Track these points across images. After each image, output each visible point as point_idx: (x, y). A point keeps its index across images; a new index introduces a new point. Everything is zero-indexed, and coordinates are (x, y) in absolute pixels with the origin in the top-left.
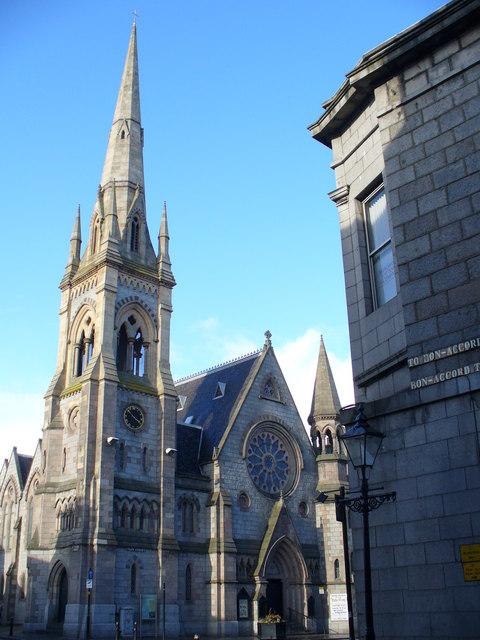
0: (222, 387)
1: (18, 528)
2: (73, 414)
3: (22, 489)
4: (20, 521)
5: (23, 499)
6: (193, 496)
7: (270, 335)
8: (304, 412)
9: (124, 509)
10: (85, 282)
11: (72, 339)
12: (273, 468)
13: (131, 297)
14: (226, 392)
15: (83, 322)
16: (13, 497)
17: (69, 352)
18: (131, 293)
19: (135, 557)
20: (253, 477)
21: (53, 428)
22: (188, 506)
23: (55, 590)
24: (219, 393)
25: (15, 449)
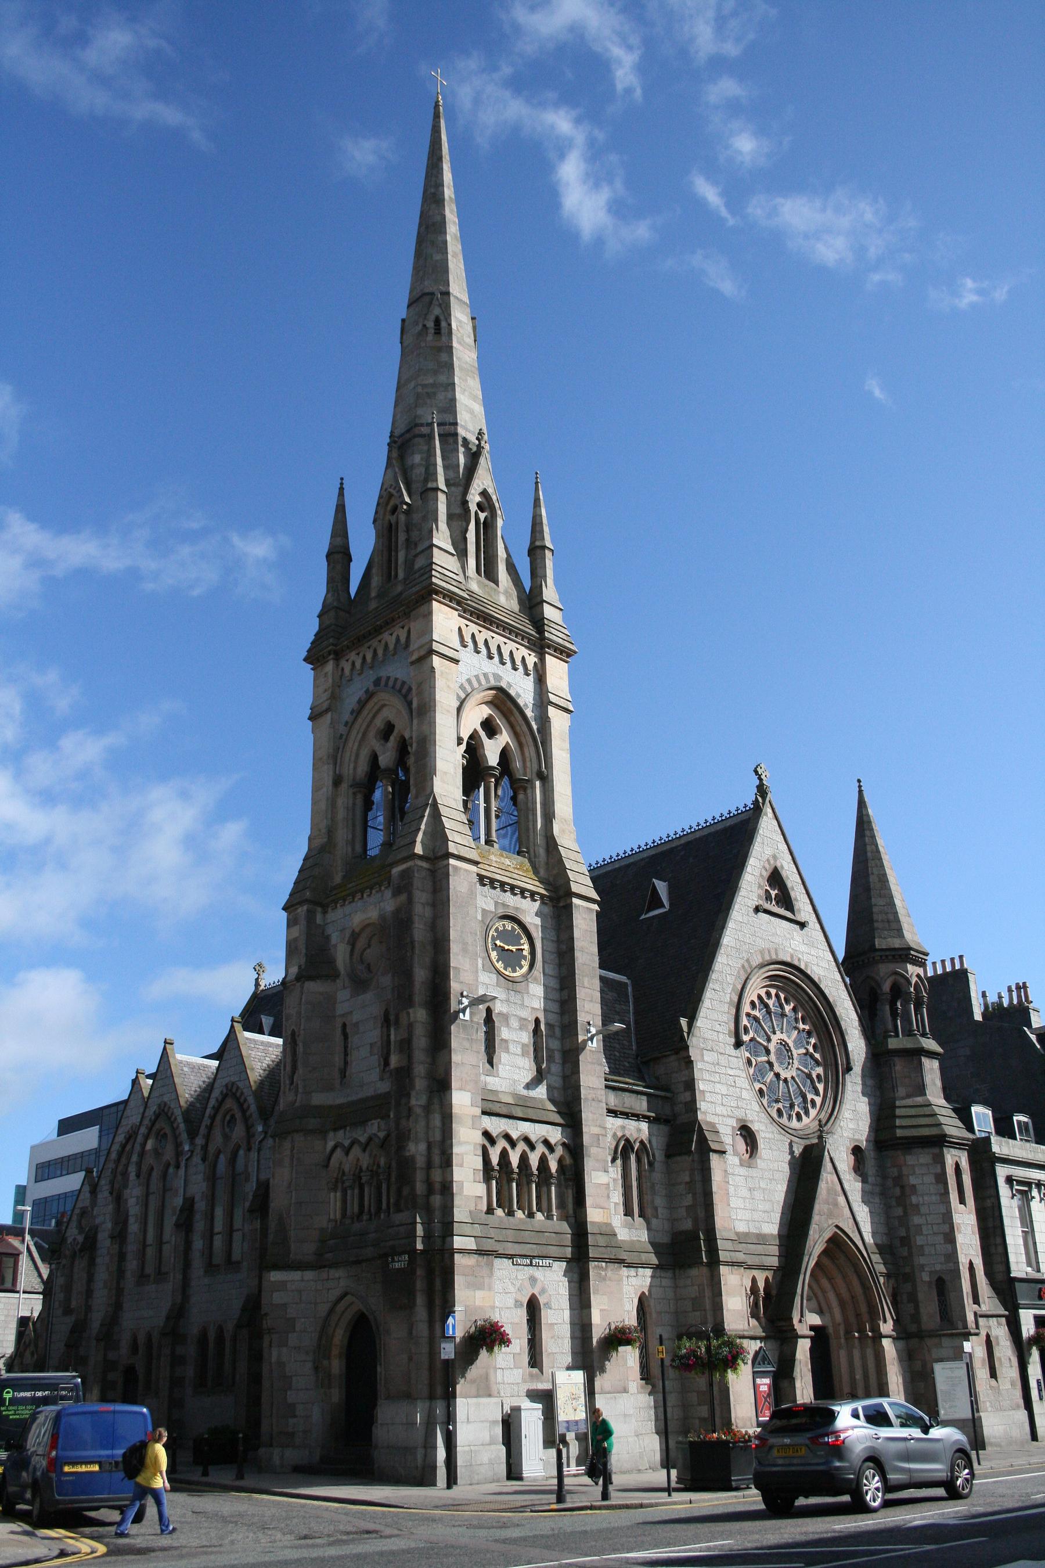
0: (662, 887)
3: (192, 1135)
4: (189, 1205)
10: (374, 643)
11: (347, 770)
13: (485, 675)
14: (671, 905)
15: (372, 733)
16: (169, 1154)
17: (340, 802)
19: (533, 1280)
21: (311, 978)
23: (336, 1366)
24: (655, 901)
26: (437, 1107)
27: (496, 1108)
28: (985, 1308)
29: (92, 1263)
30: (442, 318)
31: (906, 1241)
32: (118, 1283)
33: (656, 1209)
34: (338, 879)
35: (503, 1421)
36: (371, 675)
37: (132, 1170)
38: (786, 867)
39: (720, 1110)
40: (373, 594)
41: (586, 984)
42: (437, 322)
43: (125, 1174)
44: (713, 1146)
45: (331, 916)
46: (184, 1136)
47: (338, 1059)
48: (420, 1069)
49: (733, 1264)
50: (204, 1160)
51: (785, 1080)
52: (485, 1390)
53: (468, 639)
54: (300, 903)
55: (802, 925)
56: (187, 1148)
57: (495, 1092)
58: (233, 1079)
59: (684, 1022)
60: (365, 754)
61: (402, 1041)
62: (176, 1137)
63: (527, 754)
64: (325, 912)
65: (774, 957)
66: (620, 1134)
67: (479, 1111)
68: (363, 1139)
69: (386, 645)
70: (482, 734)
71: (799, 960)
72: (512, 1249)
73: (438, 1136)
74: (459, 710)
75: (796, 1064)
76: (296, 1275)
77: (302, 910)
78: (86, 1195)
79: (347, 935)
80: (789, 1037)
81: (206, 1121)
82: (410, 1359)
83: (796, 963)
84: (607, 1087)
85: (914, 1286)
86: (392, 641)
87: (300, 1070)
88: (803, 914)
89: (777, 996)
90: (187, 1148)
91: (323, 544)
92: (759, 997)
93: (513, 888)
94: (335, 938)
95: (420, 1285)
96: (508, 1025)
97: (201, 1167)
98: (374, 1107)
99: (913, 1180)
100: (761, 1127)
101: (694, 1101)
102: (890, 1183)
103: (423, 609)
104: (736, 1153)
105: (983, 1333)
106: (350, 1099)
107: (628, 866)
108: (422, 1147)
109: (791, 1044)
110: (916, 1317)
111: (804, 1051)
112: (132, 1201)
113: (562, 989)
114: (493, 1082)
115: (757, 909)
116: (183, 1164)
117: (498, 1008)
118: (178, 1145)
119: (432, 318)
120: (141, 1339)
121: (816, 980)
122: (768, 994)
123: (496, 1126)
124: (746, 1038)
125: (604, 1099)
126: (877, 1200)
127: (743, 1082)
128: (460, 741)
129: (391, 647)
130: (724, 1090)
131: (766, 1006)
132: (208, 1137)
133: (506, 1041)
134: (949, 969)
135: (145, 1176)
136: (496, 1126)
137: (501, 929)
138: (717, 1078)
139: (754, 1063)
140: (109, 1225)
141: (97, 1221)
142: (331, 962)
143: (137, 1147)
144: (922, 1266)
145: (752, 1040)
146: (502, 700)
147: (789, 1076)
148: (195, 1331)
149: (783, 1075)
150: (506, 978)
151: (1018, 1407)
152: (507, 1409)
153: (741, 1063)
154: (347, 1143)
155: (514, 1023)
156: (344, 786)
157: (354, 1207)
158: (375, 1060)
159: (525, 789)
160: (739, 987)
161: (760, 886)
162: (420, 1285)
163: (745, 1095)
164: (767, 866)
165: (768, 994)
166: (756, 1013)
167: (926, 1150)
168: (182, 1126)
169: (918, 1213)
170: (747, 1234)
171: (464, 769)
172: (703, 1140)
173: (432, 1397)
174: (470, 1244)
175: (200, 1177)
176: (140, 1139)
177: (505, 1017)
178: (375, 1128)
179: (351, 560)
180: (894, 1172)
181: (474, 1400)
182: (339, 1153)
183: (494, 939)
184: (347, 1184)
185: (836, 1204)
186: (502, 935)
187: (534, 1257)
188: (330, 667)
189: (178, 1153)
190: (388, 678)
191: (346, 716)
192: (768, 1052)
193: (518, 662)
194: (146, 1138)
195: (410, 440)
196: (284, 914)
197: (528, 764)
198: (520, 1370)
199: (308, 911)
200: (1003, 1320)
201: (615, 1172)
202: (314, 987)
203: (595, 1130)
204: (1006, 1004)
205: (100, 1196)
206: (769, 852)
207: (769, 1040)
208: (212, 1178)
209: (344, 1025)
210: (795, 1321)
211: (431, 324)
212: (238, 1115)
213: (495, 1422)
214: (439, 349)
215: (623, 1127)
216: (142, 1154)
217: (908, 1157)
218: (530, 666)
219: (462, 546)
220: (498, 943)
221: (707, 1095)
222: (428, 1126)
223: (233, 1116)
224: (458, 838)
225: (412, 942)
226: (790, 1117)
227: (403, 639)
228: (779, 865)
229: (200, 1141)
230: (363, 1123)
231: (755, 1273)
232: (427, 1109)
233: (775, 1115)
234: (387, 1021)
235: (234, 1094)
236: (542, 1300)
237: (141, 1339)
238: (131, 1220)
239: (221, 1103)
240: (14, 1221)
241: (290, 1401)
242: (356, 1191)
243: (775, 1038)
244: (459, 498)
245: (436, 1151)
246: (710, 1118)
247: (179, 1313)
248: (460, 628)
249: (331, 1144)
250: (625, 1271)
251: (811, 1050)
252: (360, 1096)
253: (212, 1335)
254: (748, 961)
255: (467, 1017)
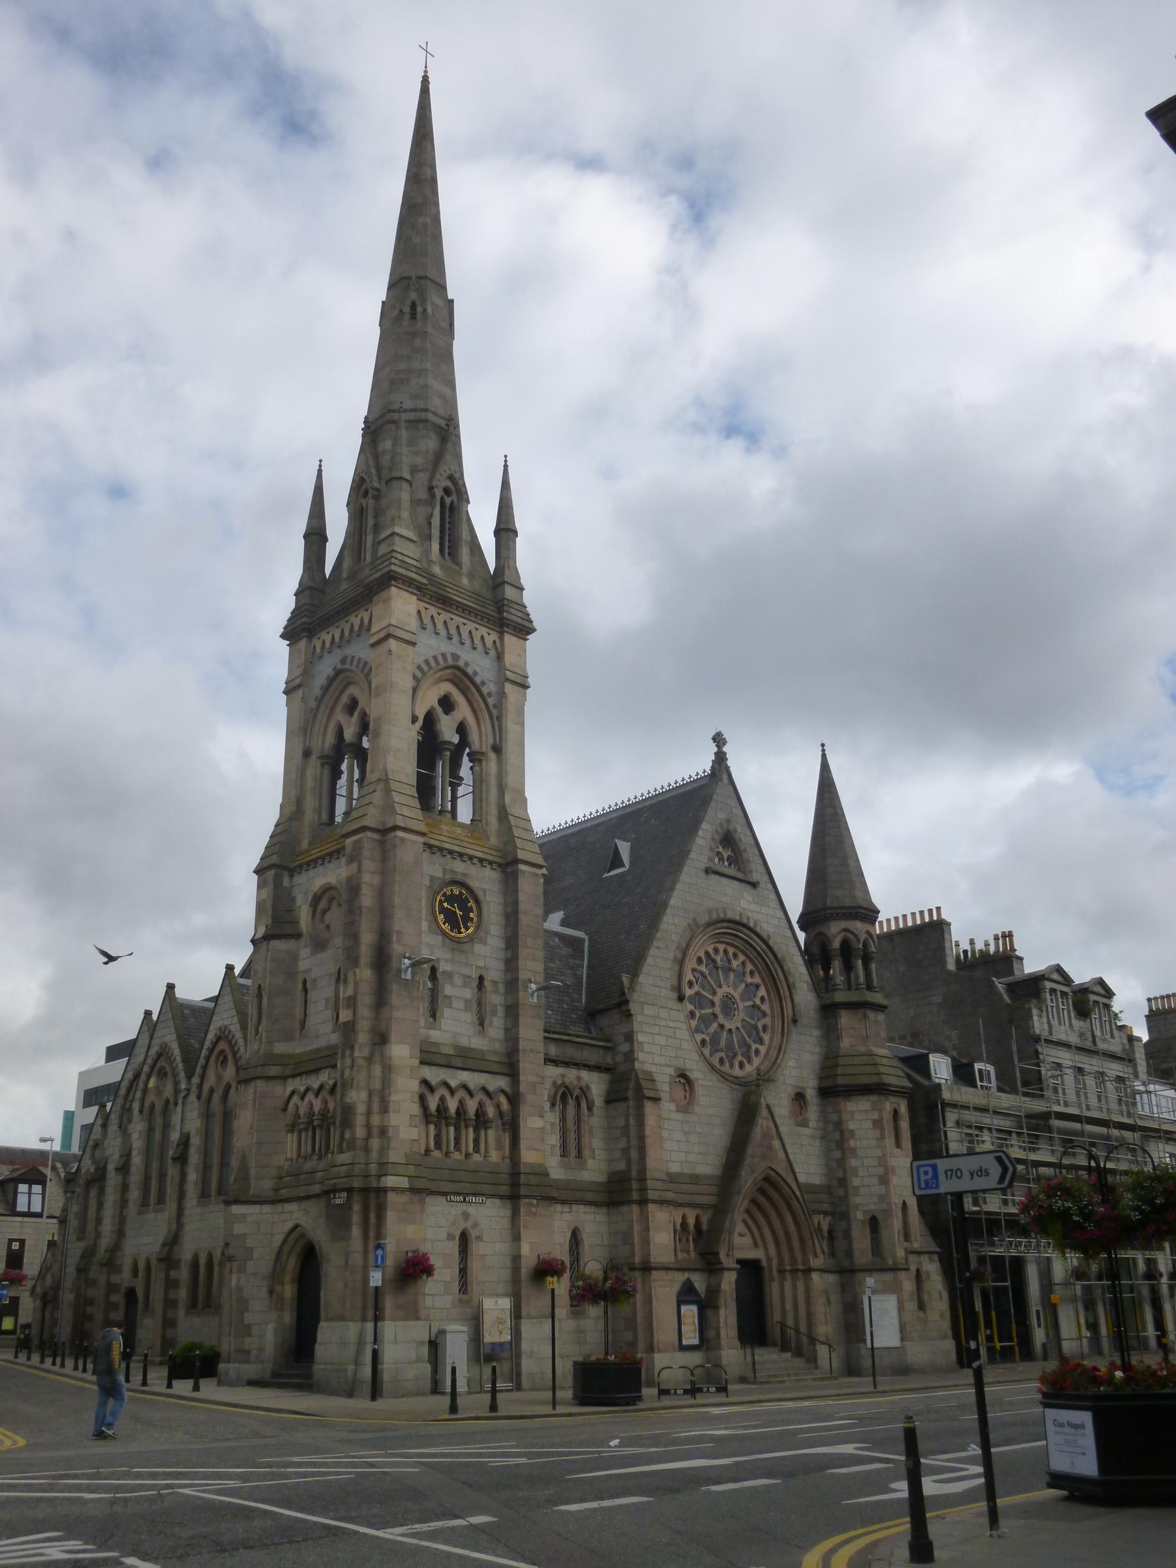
0: (624, 848)
1: (182, 1159)
2: (323, 904)
3: (189, 1077)
4: (185, 1141)
5: (193, 1097)
6: (579, 1078)
7: (724, 742)
8: (795, 904)
9: (442, 1109)
10: (342, 623)
12: (741, 1015)
13: (444, 655)
14: (632, 863)
16: (168, 1091)
18: (447, 647)
19: (466, 1216)
20: (699, 1037)
22: (571, 1103)
23: (289, 1291)
24: (616, 861)
25: (171, 987)
26: (377, 1058)
27: (438, 1059)
28: (916, 1246)
29: (102, 1191)
30: (418, 303)
31: (843, 1182)
32: (121, 1213)
33: (593, 1150)
34: (305, 844)
35: (430, 1342)
36: (338, 654)
37: (136, 1106)
38: (739, 829)
39: (657, 1060)
40: (345, 575)
41: (529, 944)
42: (413, 306)
43: (130, 1110)
44: (647, 1093)
45: (298, 879)
46: (182, 1075)
47: (299, 1012)
48: (364, 1025)
49: (662, 1202)
50: (199, 1097)
51: (730, 1031)
52: (412, 1313)
53: (427, 621)
54: (270, 867)
55: (754, 885)
56: (183, 1086)
57: (436, 1044)
58: (225, 1023)
59: (625, 979)
60: (332, 727)
61: (349, 998)
62: (175, 1075)
63: (483, 729)
64: (291, 876)
65: (722, 916)
66: (559, 1082)
67: (417, 1062)
68: (316, 1086)
69: (352, 625)
70: (439, 710)
71: (748, 918)
72: (445, 1187)
73: (377, 1085)
74: (415, 690)
75: (742, 1015)
76: (254, 1209)
77: (270, 874)
78: (97, 1129)
79: (310, 898)
80: (735, 990)
81: (202, 1061)
82: (346, 1286)
83: (745, 921)
84: (545, 1038)
85: (849, 1225)
86: (356, 622)
87: (264, 1022)
88: (754, 875)
89: (725, 951)
90: (183, 1086)
91: (301, 525)
92: (707, 953)
93: (461, 855)
94: (300, 900)
95: (356, 1218)
96: (452, 983)
97: (196, 1104)
98: (326, 1059)
99: (852, 1125)
100: (699, 1073)
101: (632, 1051)
102: (831, 1127)
103: (384, 595)
104: (672, 1100)
105: (913, 1268)
106: (308, 1049)
107: (599, 825)
108: (364, 1095)
109: (737, 997)
110: (849, 1254)
111: (751, 1003)
112: (135, 1136)
113: (507, 948)
114: (435, 1035)
115: (708, 871)
116: (180, 1101)
117: (443, 967)
118: (176, 1083)
119: (409, 303)
120: (142, 1265)
121: (765, 937)
122: (716, 951)
123: (434, 1075)
124: (688, 992)
125: (542, 1049)
126: (818, 1143)
127: (684, 1034)
128: (414, 719)
129: (356, 628)
130: (663, 1041)
131: (714, 961)
132: (203, 1077)
133: (450, 997)
134: (910, 924)
135: (149, 1113)
136: (434, 1075)
137: (449, 893)
138: (656, 1030)
139: (698, 1015)
140: (117, 1157)
141: (108, 1153)
142: (295, 922)
143: (141, 1084)
144: (857, 1206)
145: (697, 994)
146: (461, 677)
147: (733, 1027)
148: (186, 1256)
149: (728, 1026)
150: (452, 939)
151: (946, 1337)
152: (434, 1330)
153: (682, 1016)
154: (302, 1089)
155: (458, 981)
156: (314, 757)
157: (307, 1148)
158: (329, 1013)
159: (480, 761)
160: (684, 945)
161: (711, 849)
162: (356, 1218)
163: (685, 1045)
164: (719, 829)
165: (716, 951)
166: (703, 968)
167: (865, 1098)
168: (181, 1066)
169: (856, 1156)
170: (681, 1174)
171: (419, 743)
172: (639, 1089)
173: (364, 1319)
174: (404, 1183)
175: (195, 1114)
176: (143, 1077)
177: (449, 975)
178: (325, 1077)
179: (326, 540)
180: (834, 1117)
181: (402, 1323)
182: (295, 1099)
183: (441, 902)
184: (315, 1123)
185: (770, 1148)
186: (451, 899)
187: (468, 1194)
188: (303, 643)
189: (177, 1091)
190: (353, 657)
191: (317, 692)
192: (713, 1004)
193: (477, 641)
194: (149, 1076)
195: (382, 426)
196: (255, 877)
197: (484, 738)
198: (450, 1297)
199: (276, 875)
200: (936, 1257)
201: (553, 1117)
202: (280, 946)
203: (532, 1079)
204: (992, 949)
205: (109, 1129)
206: (722, 816)
207: (715, 993)
208: (207, 1115)
209: (305, 981)
210: (722, 1256)
211: (407, 309)
212: (230, 1057)
213: (421, 1343)
214: (414, 335)
215: (563, 1076)
216: (145, 1091)
217: (848, 1104)
218: (489, 644)
219: (427, 531)
220: (445, 905)
221: (645, 1046)
222: (369, 1077)
223: (225, 1057)
224: (406, 812)
225: (360, 907)
226: (732, 1066)
227: (366, 622)
228: (731, 828)
229: (196, 1080)
230: (316, 1071)
231: (687, 1211)
232: (370, 1059)
233: (717, 1065)
234: (340, 978)
235: (227, 1037)
236: (473, 1234)
237: (142, 1265)
238: (134, 1153)
239: (215, 1044)
240: (63, 1146)
241: (246, 1321)
242: (310, 1133)
243: (720, 992)
244: (426, 483)
245: (376, 1099)
246: (648, 1067)
247: (173, 1240)
248: (419, 612)
249: (289, 1090)
250: (559, 1208)
251: (758, 1002)
252: (316, 1046)
253: (203, 1261)
254: (694, 920)
255: (409, 977)
